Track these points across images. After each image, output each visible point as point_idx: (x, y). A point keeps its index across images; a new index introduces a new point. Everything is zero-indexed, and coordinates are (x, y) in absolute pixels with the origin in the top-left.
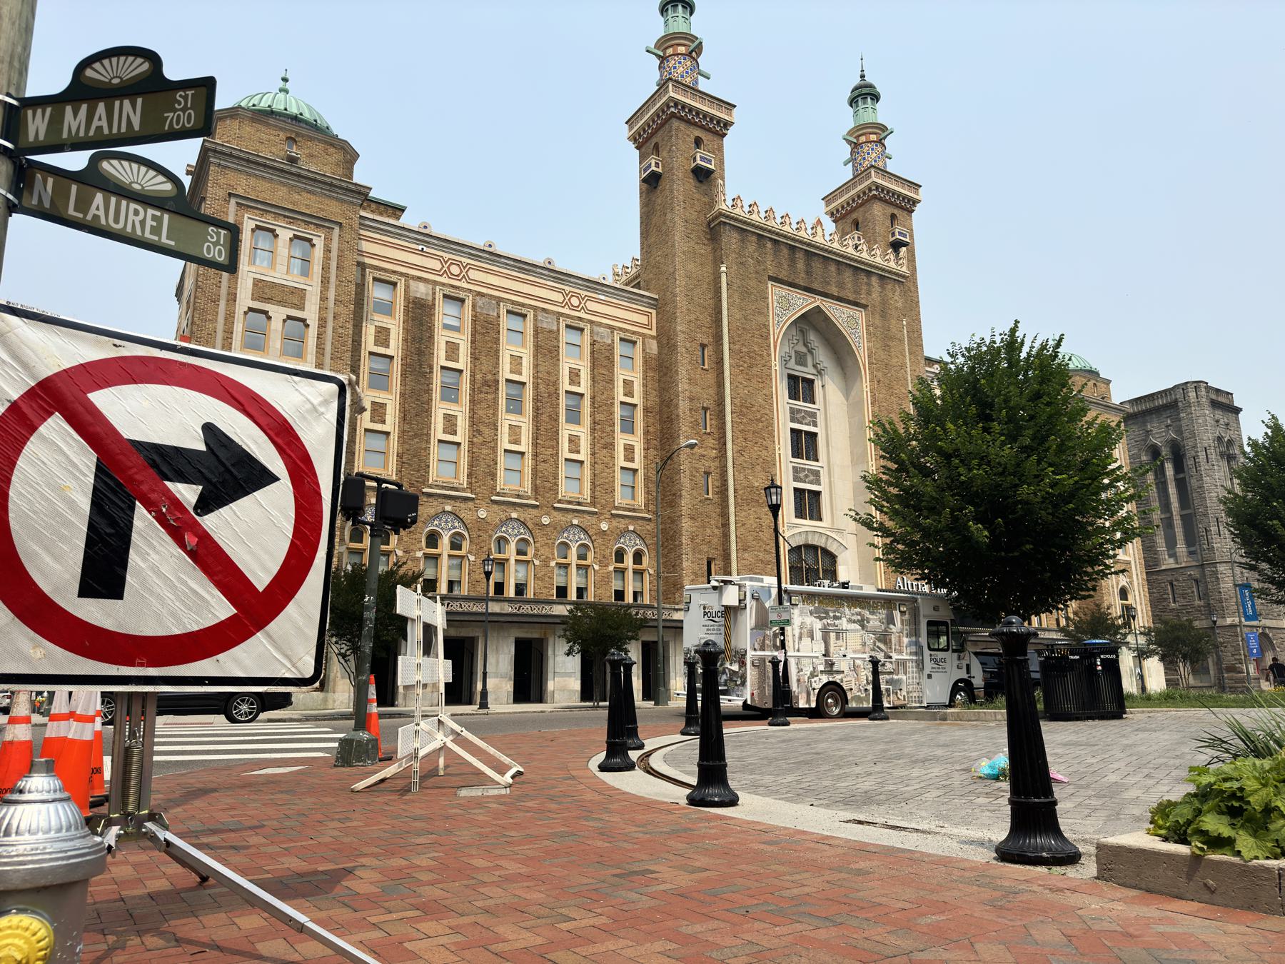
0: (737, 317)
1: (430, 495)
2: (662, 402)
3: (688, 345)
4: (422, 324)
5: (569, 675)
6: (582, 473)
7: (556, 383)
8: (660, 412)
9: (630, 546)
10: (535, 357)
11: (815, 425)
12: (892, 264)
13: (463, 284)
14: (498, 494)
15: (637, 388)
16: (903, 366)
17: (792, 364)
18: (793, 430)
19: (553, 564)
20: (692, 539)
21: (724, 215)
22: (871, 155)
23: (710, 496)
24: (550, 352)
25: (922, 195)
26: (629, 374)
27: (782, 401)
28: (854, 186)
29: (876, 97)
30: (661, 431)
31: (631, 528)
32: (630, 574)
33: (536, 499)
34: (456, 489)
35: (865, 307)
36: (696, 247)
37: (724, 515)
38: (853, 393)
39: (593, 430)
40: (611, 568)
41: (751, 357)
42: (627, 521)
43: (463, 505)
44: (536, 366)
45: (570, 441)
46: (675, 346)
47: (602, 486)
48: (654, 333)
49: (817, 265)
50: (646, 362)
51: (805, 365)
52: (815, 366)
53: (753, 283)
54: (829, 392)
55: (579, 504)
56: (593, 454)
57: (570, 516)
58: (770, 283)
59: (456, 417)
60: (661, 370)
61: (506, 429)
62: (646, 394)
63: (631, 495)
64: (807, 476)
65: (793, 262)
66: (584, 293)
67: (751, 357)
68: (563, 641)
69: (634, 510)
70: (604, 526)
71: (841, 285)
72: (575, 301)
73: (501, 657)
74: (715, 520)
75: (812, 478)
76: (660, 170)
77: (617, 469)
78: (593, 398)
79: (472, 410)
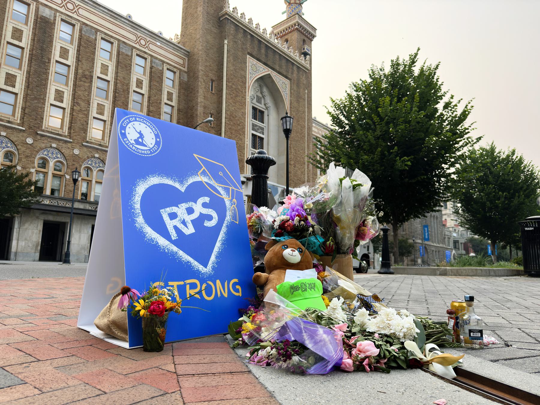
0: (232, 68)
1: (42, 136)
3: (205, 78)
4: (45, 32)
7: (128, 85)
11: (263, 134)
12: (303, 62)
13: (75, 16)
14: (87, 142)
15: (175, 97)
16: (304, 112)
17: (255, 101)
18: (253, 135)
21: (228, 15)
24: (126, 67)
25: (318, 33)
27: (249, 120)
34: (61, 135)
41: (237, 91)
43: (64, 145)
44: (117, 73)
46: (198, 77)
48: (186, 69)
49: (270, 53)
50: (180, 84)
51: (261, 103)
52: (265, 105)
53: (240, 54)
58: (248, 56)
59: (63, 92)
61: (95, 105)
62: (179, 101)
66: (148, 39)
67: (237, 91)
71: (280, 66)
72: (143, 42)
73: (82, 235)
78: (149, 97)
79: (74, 90)
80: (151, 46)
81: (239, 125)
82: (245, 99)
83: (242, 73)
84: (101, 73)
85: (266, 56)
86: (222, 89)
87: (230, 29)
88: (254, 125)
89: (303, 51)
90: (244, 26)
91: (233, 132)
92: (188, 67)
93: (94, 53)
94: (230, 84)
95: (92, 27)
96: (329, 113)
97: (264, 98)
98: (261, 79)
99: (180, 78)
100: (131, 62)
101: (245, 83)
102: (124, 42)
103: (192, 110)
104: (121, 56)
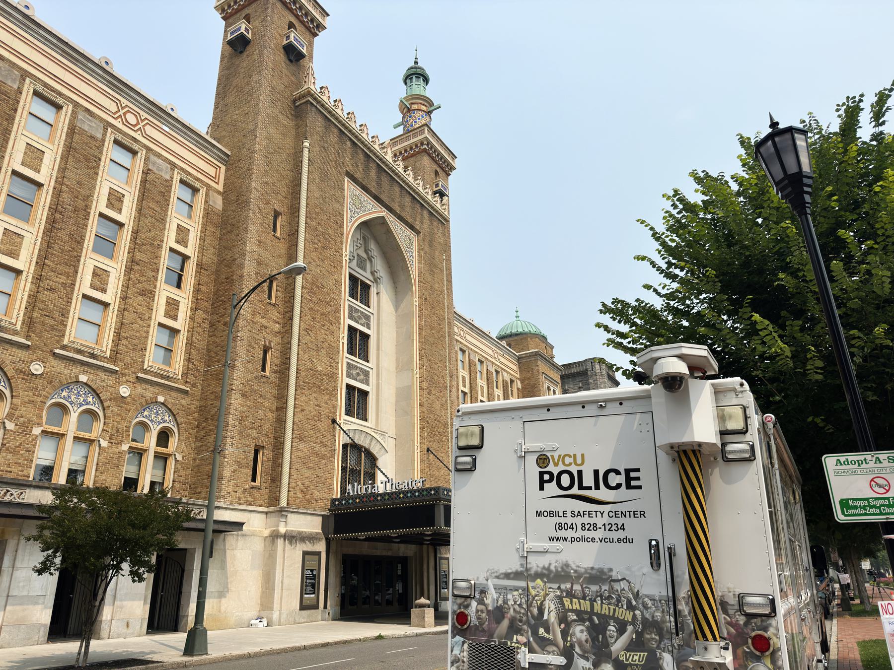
2: (221, 262)
3: (262, 206)
5: (33, 600)
6: (105, 319)
7: (88, 198)
8: (217, 272)
9: (158, 421)
10: (65, 158)
15: (193, 238)
16: (442, 292)
17: (354, 264)
18: (350, 327)
19: (37, 431)
20: (241, 421)
21: (312, 96)
22: (419, 119)
23: (267, 373)
24: (87, 160)
26: (184, 224)
28: (402, 141)
29: (426, 80)
30: (216, 293)
31: (161, 399)
32: (149, 459)
33: (28, 337)
35: (418, 232)
36: (280, 116)
37: (282, 397)
38: (402, 306)
39: (129, 270)
40: (125, 447)
42: (156, 390)
44: (63, 170)
45: (95, 274)
46: (247, 202)
47: (129, 338)
48: (220, 188)
49: (385, 181)
51: (365, 270)
52: (372, 273)
54: (382, 298)
55: (93, 356)
56: (124, 298)
57: (75, 370)
58: (346, 179)
60: (225, 227)
62: (202, 249)
63: (166, 356)
64: (358, 374)
65: (367, 169)
68: (37, 546)
69: (168, 378)
70: (124, 391)
71: (402, 206)
74: (269, 403)
75: (362, 377)
76: (249, 36)
77: (154, 324)
80: (149, 130)
81: (328, 303)
82: (341, 256)
83: (337, 206)
84: (23, 164)
85: (379, 184)
86: (297, 231)
87: (315, 122)
88: (352, 310)
89: (435, 189)
90: (340, 122)
91: (318, 316)
92: (225, 185)
93: (11, 119)
94: (314, 224)
95: (14, 65)
96: (656, 236)
97: (371, 261)
98: (365, 225)
99: (206, 202)
100: (101, 153)
101: (341, 226)
102: (87, 110)
103: (229, 266)
104: (76, 137)
